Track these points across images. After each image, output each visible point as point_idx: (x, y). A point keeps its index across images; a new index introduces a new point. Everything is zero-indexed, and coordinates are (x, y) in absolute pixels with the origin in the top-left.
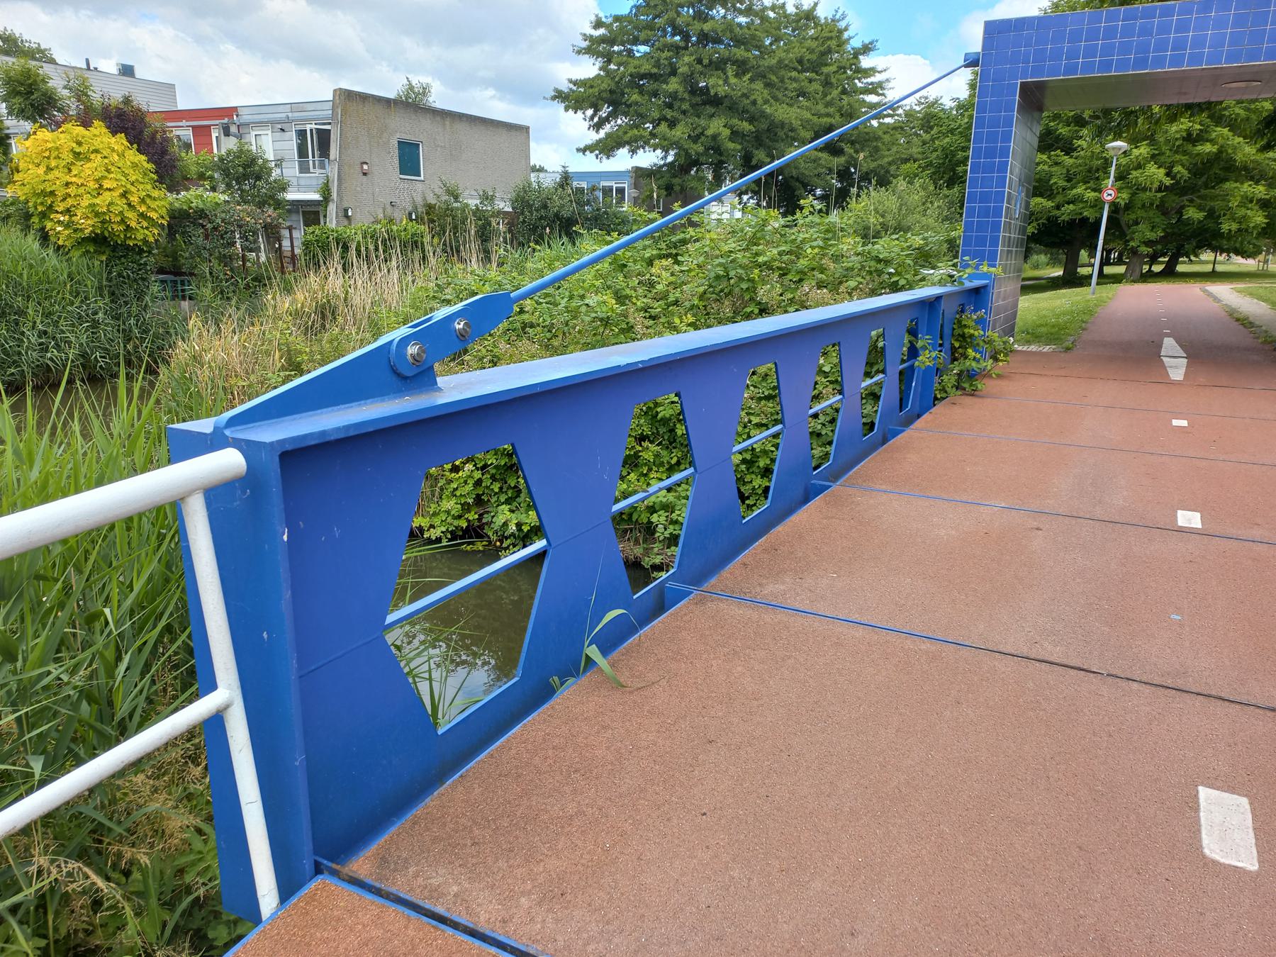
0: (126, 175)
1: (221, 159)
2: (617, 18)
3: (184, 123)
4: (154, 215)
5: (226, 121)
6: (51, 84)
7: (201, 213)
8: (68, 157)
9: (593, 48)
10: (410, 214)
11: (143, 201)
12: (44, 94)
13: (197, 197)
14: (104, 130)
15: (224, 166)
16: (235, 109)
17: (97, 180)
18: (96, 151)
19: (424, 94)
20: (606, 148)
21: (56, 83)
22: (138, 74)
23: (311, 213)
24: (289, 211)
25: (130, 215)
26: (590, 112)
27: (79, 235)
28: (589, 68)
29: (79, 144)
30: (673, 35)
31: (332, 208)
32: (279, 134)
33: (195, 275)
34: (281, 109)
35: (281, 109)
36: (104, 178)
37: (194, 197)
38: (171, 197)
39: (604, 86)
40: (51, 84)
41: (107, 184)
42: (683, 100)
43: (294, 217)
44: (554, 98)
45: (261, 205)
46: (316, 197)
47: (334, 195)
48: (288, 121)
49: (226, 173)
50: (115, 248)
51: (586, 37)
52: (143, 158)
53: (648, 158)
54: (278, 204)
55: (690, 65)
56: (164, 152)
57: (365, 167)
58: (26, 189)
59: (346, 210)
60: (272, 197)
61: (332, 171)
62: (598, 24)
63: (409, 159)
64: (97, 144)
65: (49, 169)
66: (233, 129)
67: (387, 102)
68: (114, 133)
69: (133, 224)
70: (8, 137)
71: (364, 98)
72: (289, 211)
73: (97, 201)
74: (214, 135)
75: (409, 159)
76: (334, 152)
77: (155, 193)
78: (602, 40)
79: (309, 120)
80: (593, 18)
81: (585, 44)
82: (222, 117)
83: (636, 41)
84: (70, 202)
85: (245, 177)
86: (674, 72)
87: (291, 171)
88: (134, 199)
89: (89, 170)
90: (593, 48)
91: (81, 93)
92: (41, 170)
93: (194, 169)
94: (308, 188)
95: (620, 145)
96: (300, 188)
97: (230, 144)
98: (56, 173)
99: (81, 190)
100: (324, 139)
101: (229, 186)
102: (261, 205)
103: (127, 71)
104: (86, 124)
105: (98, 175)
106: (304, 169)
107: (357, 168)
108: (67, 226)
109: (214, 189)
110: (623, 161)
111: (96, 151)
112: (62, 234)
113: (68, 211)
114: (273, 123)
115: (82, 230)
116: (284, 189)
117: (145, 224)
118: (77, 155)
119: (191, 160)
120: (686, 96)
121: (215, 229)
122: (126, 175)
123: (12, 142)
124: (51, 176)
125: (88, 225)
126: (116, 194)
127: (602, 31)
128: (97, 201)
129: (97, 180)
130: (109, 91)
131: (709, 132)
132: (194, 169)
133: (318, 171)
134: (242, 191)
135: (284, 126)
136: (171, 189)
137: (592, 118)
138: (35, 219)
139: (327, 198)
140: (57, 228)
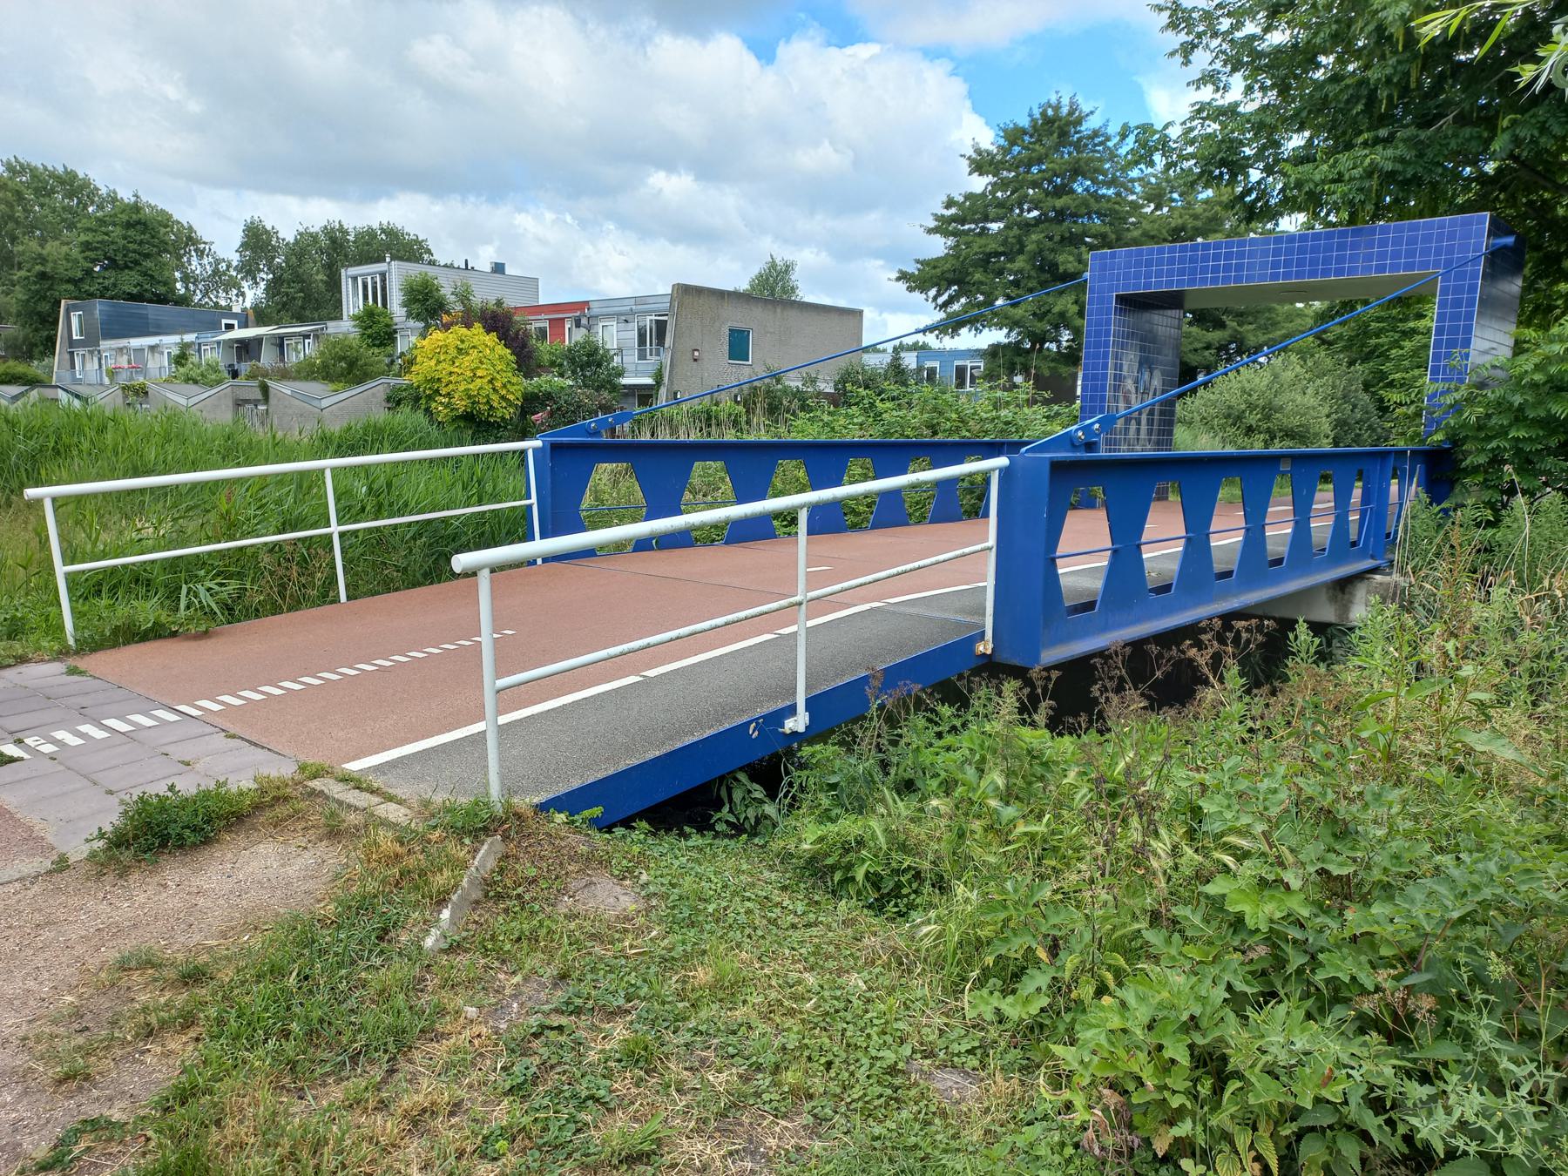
0: (494, 365)
1: (570, 350)
2: (969, 196)
3: (543, 316)
4: (511, 397)
5: (578, 314)
6: (443, 291)
7: (549, 396)
8: (453, 352)
9: (943, 226)
10: (736, 396)
11: (504, 386)
12: (437, 301)
13: (546, 382)
14: (482, 330)
15: (571, 355)
16: (587, 303)
17: (472, 370)
18: (474, 347)
19: (786, 271)
20: (951, 326)
21: (447, 292)
22: (508, 271)
23: (644, 395)
24: (626, 395)
25: (494, 397)
26: (933, 292)
27: (455, 413)
28: (938, 246)
29: (463, 341)
30: (1151, 164)
31: (663, 391)
32: (622, 325)
33: (505, 1094)
34: (626, 302)
35: (626, 302)
36: (478, 368)
37: (548, 381)
38: (526, 382)
39: (948, 266)
40: (443, 291)
41: (479, 373)
42: (1029, 277)
43: (630, 400)
44: (898, 279)
45: (598, 389)
46: (649, 381)
47: (666, 380)
48: (632, 312)
49: (572, 361)
50: (480, 423)
51: (938, 218)
52: (508, 351)
53: (995, 336)
54: (614, 388)
55: (1038, 242)
56: (524, 345)
57: (696, 354)
58: (420, 377)
59: (675, 394)
60: (610, 382)
61: (666, 358)
62: (950, 203)
63: (738, 346)
64: (475, 341)
65: (439, 362)
66: (584, 321)
67: (721, 295)
68: (488, 332)
69: (495, 405)
70: (395, 331)
71: (699, 291)
72: (626, 395)
73: (471, 386)
74: (567, 326)
75: (738, 346)
76: (668, 341)
77: (514, 380)
78: (953, 219)
79: (649, 312)
80: (945, 199)
81: (932, 224)
82: (575, 310)
83: (986, 219)
84: (451, 387)
85: (588, 364)
86: (1021, 252)
87: (631, 358)
88: (498, 384)
89: (467, 362)
90: (943, 226)
91: (464, 298)
92: (433, 363)
93: (546, 357)
94: (644, 374)
95: (961, 324)
96: (637, 374)
97: (579, 335)
98: (443, 364)
99: (460, 378)
100: (661, 327)
101: (574, 372)
102: (598, 389)
103: (498, 268)
104: (468, 326)
105: (473, 366)
106: (642, 356)
107: (689, 355)
108: (446, 406)
109: (561, 375)
110: (967, 339)
111: (474, 347)
112: (442, 413)
113: (449, 394)
114: (619, 314)
115: (457, 409)
116: (620, 374)
117: (504, 404)
118: (460, 350)
119: (544, 349)
120: (1033, 273)
121: (559, 409)
122: (494, 365)
123: (398, 336)
124: (439, 367)
125: (461, 405)
126: (485, 380)
127: (953, 211)
128: (471, 386)
129: (472, 370)
130: (483, 295)
131: (1056, 310)
132: (546, 357)
133: (654, 358)
134: (585, 376)
135: (629, 318)
136: (528, 376)
137: (935, 299)
138: (423, 401)
139: (659, 383)
140: (439, 407)
